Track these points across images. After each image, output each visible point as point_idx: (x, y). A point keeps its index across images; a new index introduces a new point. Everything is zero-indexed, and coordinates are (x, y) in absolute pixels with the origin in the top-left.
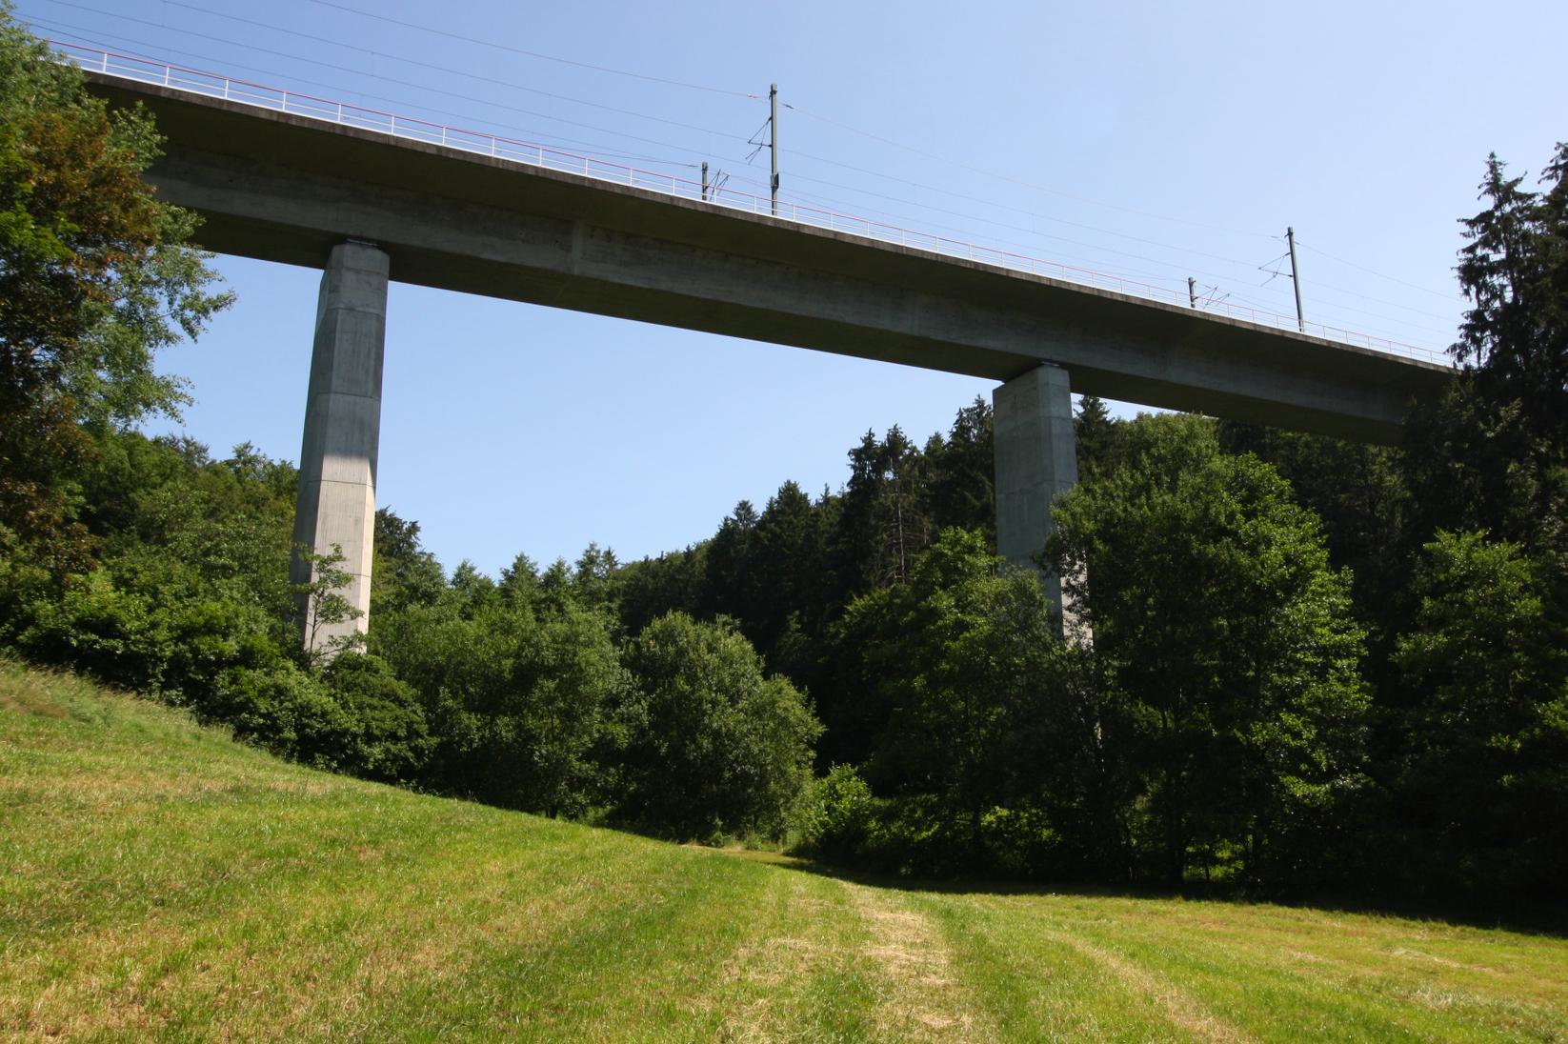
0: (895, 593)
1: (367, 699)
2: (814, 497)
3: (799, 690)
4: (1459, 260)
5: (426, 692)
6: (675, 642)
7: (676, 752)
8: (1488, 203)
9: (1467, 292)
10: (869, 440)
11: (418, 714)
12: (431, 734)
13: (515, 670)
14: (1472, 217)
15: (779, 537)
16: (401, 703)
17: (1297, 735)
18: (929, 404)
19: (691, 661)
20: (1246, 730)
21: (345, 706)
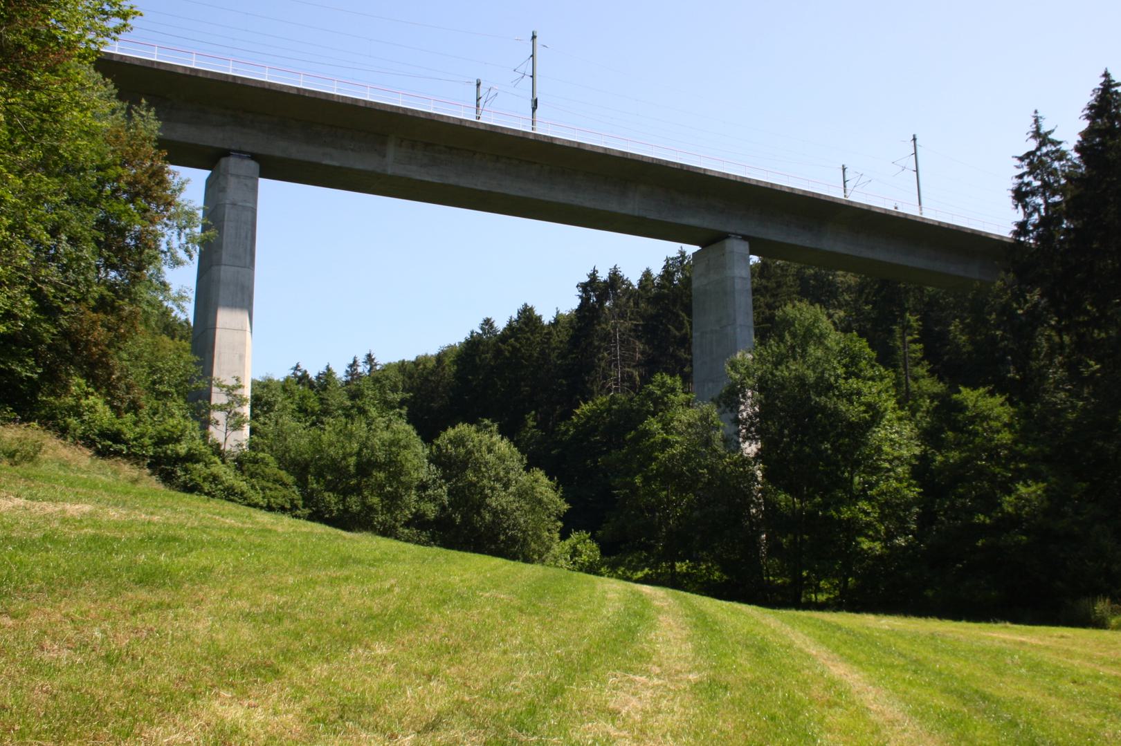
0: (613, 400)
1: (265, 484)
2: (548, 318)
3: (551, 479)
4: (1013, 183)
5: (299, 479)
6: (464, 446)
7: (466, 521)
8: (1033, 145)
9: (1017, 207)
10: (593, 276)
11: (296, 493)
12: (304, 507)
13: (358, 465)
14: (1021, 154)
15: (519, 350)
16: (284, 485)
17: (867, 514)
18: (640, 257)
19: (476, 459)
20: (838, 511)
21: (253, 487)
